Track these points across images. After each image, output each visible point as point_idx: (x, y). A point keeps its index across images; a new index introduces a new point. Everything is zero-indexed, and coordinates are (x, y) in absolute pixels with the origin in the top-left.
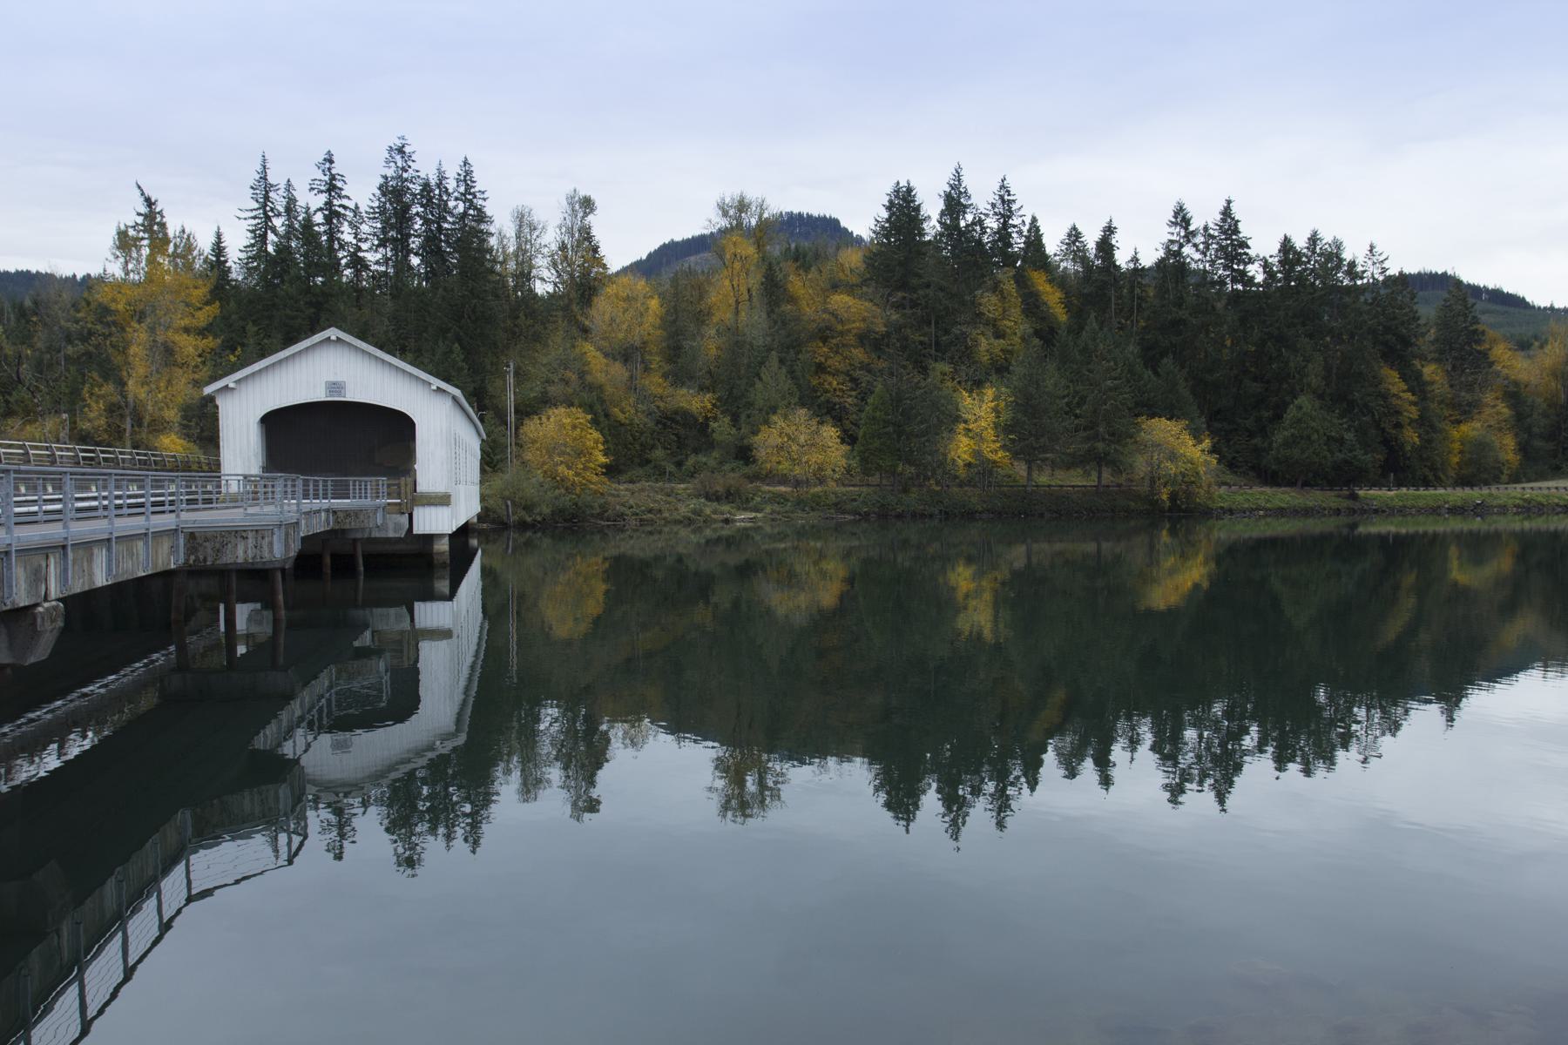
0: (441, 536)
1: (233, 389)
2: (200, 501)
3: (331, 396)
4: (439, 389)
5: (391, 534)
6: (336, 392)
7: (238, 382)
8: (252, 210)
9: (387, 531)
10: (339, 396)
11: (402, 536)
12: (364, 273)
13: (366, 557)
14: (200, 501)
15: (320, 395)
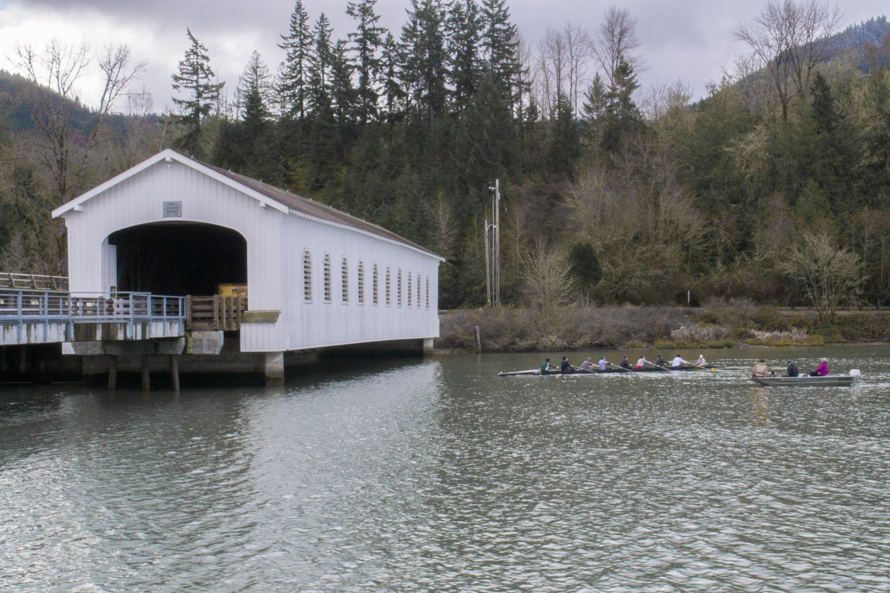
0: (274, 354)
1: (79, 212)
2: (61, 313)
3: (168, 216)
4: (268, 207)
5: (206, 351)
6: (173, 212)
7: (84, 204)
8: (529, 47)
9: (202, 348)
10: (176, 216)
11: (217, 353)
12: (332, 106)
13: (182, 375)
14: (61, 313)
15: (158, 216)
